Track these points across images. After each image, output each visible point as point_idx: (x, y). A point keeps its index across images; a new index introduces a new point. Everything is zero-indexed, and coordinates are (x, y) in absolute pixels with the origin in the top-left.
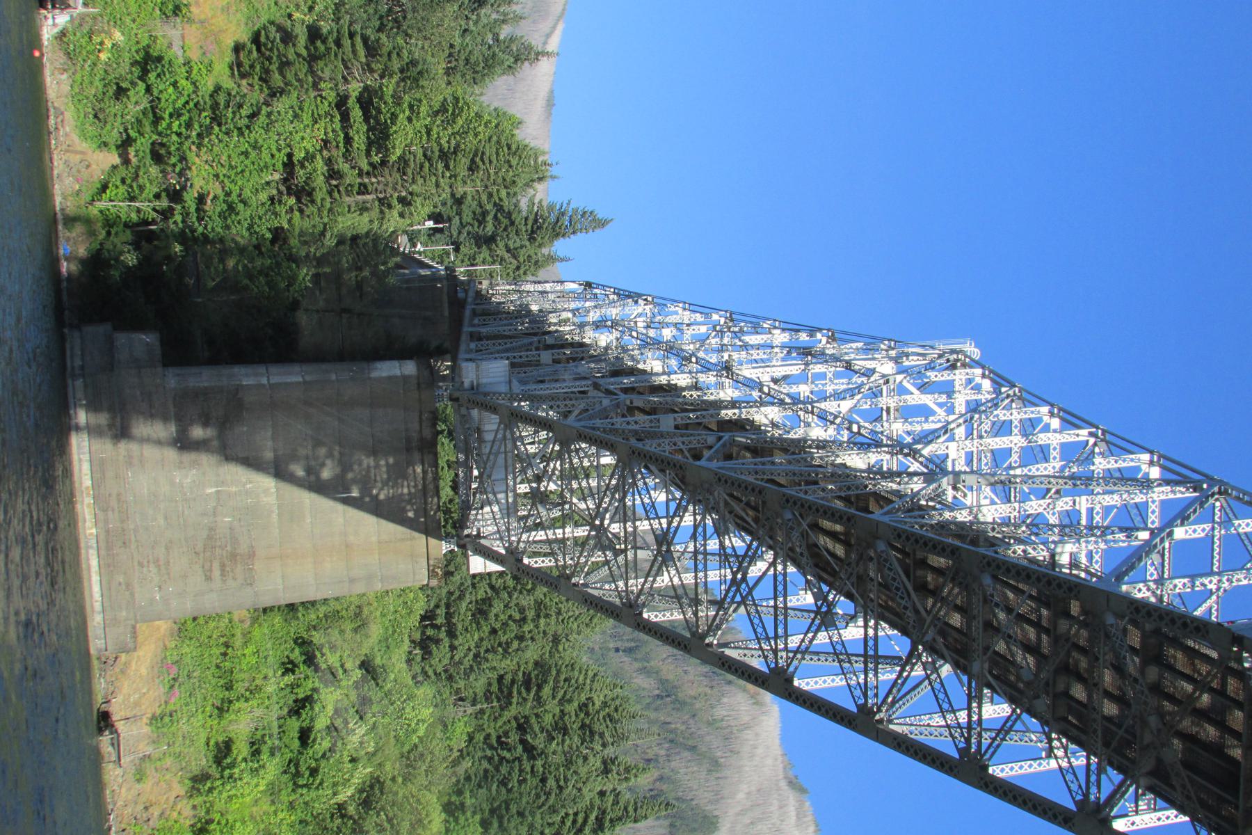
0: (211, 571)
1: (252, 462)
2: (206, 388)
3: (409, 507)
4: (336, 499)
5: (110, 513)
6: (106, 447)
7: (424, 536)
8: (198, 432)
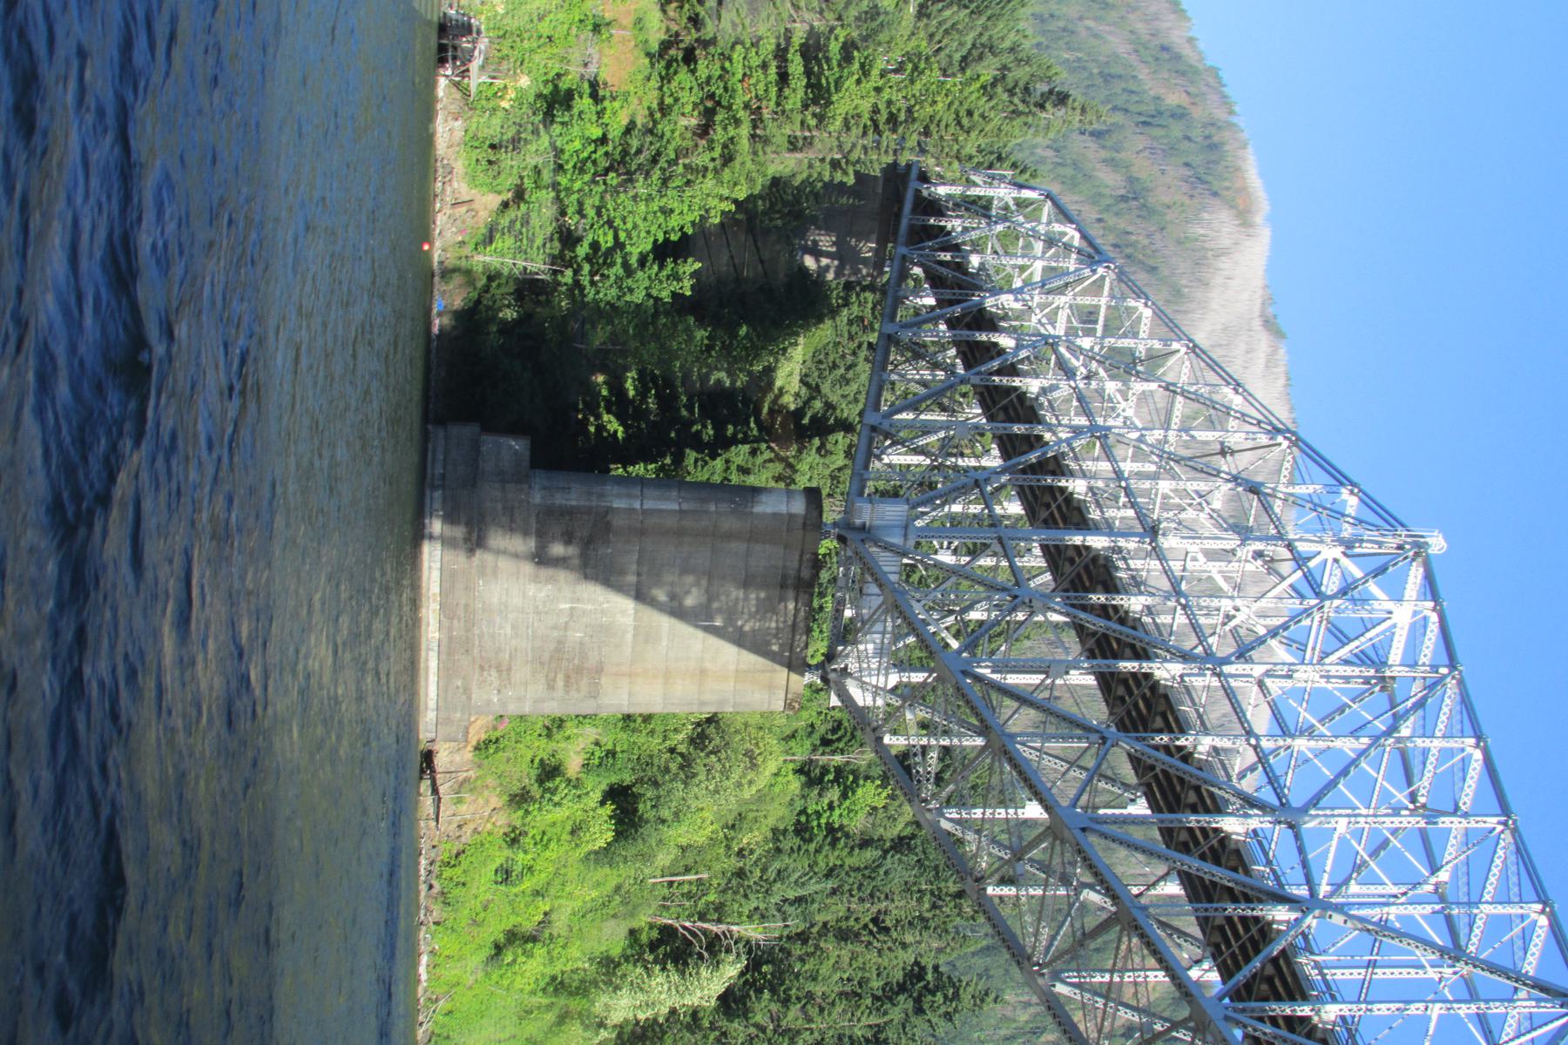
0: (554, 680)
1: (620, 589)
2: (572, 507)
3: (774, 641)
4: (697, 626)
5: (455, 621)
6: (459, 559)
7: (786, 670)
8: (558, 549)
